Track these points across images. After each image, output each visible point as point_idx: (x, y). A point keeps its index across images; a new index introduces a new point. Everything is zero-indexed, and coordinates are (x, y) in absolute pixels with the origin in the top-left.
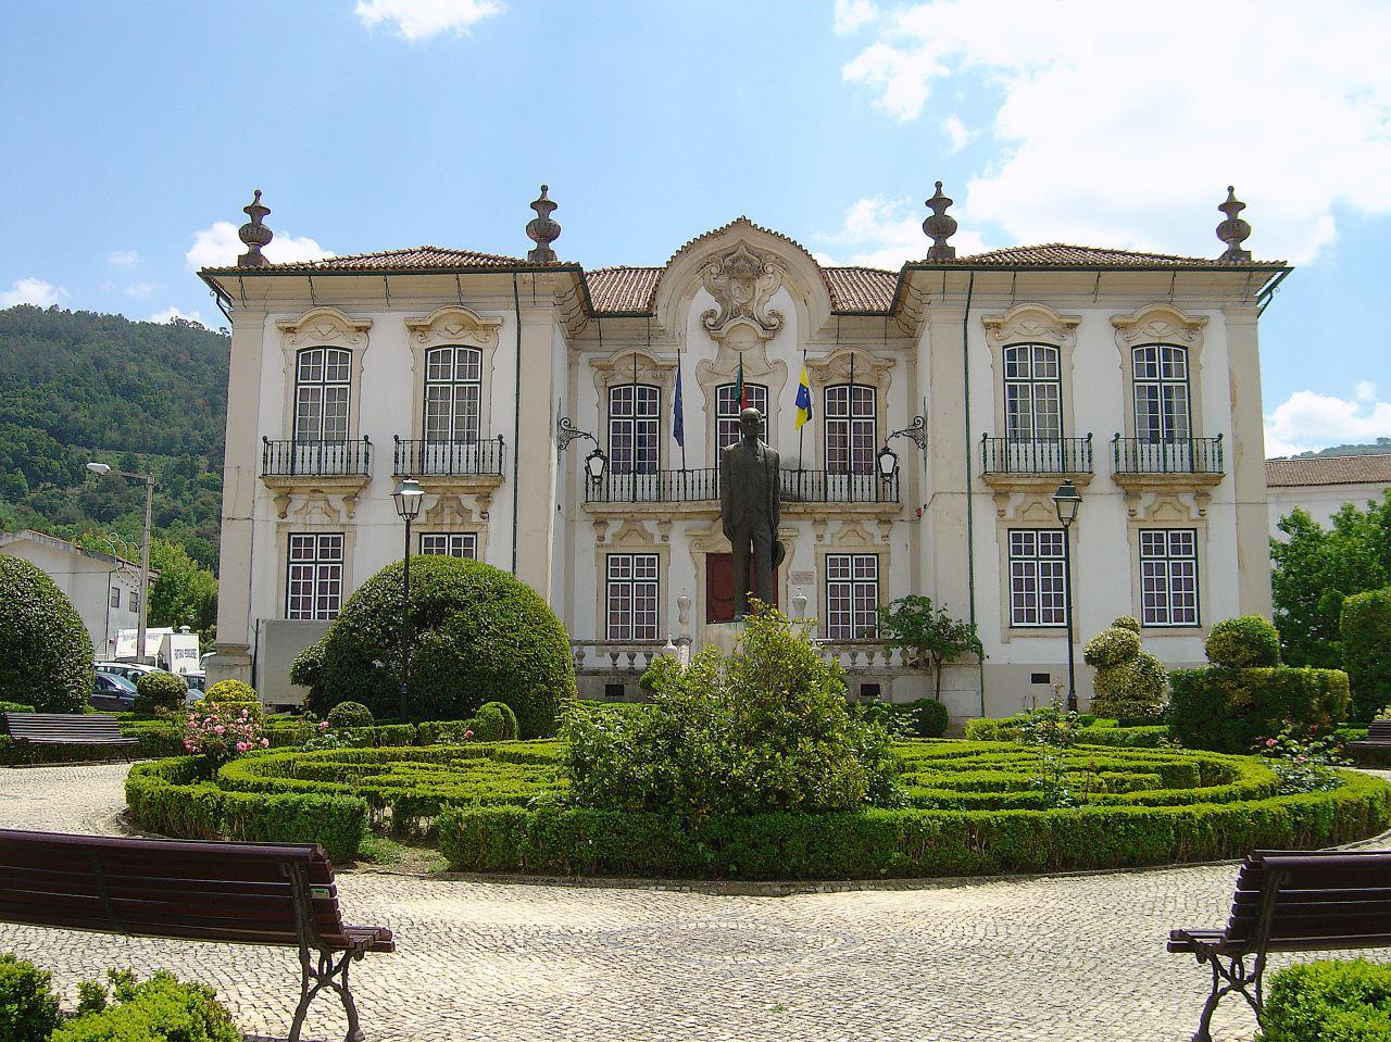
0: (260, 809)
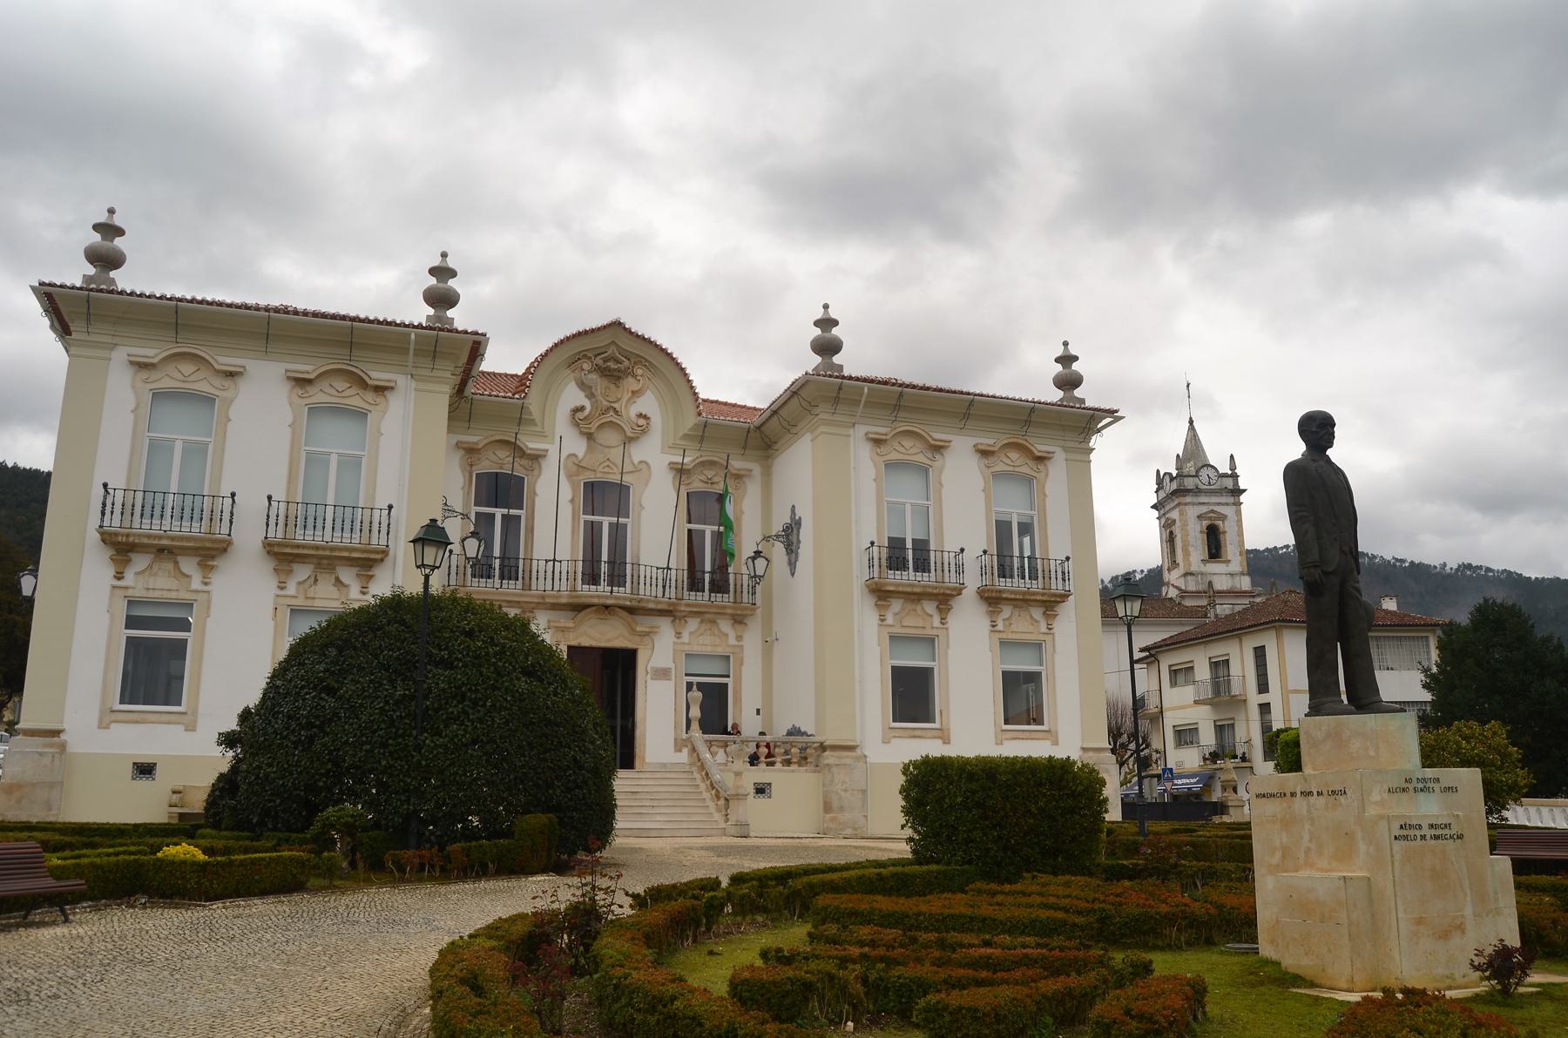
0: (880, 877)
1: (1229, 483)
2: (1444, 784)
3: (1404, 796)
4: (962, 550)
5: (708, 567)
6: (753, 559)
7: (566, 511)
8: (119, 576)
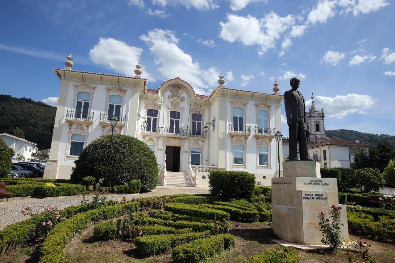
1: (321, 115)
2: (324, 182)
3: (310, 186)
4: (250, 126)
5: (196, 130)
6: (205, 128)
7: (166, 118)
8: (70, 129)
